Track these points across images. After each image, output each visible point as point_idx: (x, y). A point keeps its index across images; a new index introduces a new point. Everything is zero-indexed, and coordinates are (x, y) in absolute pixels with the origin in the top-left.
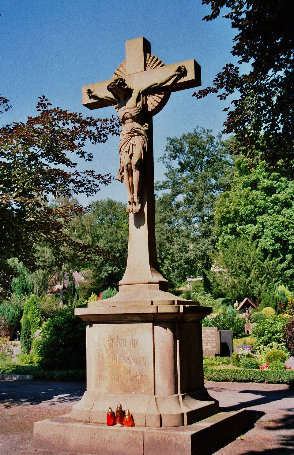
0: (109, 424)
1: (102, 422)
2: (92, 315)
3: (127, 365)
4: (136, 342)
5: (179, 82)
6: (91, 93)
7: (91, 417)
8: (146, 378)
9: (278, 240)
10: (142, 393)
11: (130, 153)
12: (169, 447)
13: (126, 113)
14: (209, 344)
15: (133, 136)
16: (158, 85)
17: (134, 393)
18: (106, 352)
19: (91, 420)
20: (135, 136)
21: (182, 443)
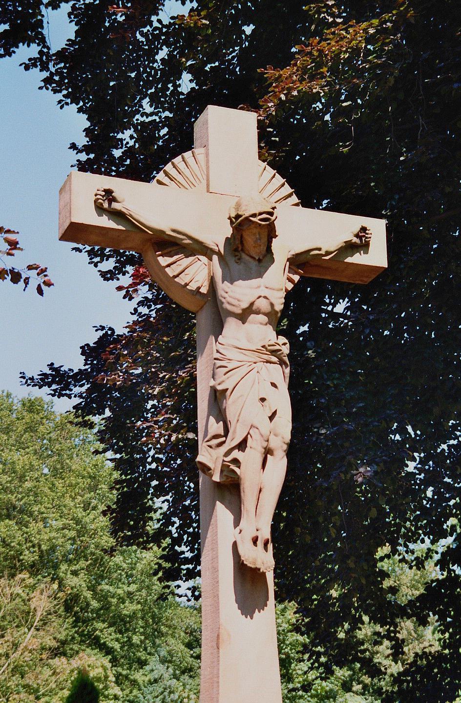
5: (349, 260)
20: (271, 362)
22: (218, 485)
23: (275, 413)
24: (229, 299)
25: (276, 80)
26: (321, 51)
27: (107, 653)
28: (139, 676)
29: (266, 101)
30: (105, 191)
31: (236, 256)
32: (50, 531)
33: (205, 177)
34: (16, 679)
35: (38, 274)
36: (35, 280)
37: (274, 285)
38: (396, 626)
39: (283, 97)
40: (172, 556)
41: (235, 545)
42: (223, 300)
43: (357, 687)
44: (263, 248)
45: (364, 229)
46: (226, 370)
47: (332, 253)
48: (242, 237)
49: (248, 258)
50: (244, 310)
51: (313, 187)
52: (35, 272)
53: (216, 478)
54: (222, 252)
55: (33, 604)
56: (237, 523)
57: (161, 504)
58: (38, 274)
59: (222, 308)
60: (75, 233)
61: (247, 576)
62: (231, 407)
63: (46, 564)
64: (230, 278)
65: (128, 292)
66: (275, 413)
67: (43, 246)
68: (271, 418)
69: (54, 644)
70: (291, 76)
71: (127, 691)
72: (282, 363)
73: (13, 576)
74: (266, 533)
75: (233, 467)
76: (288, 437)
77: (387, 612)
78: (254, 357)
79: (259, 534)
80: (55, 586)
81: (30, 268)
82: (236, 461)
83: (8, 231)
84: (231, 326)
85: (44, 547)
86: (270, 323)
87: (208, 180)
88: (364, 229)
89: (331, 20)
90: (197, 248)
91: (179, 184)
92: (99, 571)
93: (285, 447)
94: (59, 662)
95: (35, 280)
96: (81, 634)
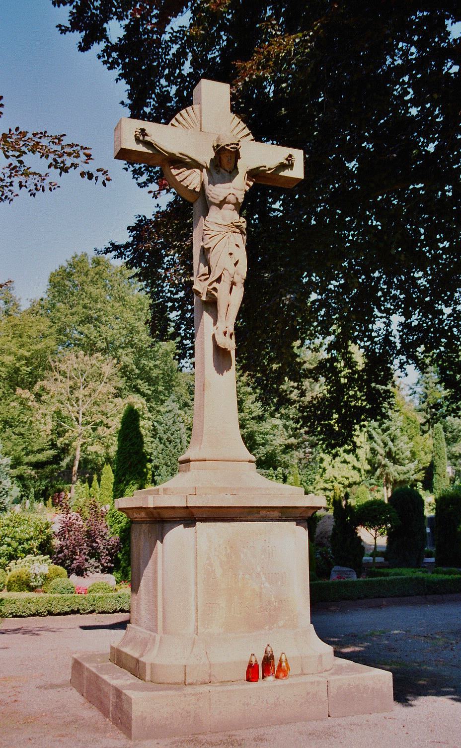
0: (248, 680)
1: (226, 680)
2: (218, 507)
5: (282, 174)
17: (267, 628)
18: (221, 567)
19: (213, 679)
20: (236, 232)
21: (381, 687)
22: (205, 303)
23: (237, 262)
24: (212, 195)
25: (243, 69)
26: (269, 52)
27: (144, 396)
28: (162, 409)
29: (238, 82)
30: (141, 129)
31: (216, 169)
32: (113, 331)
33: (199, 122)
34: (95, 408)
35: (103, 174)
36: (102, 178)
37: (238, 187)
38: (302, 382)
39: (247, 79)
40: (181, 346)
41: (214, 336)
42: (209, 196)
43: (278, 415)
44: (233, 165)
45: (290, 156)
46: (210, 236)
47: (272, 169)
48: (220, 158)
49: (223, 171)
50: (221, 202)
51: (262, 131)
52: (101, 173)
53: (204, 298)
54: (209, 167)
55: (103, 370)
56: (215, 324)
57: (174, 315)
58: (103, 174)
59: (208, 200)
60: (123, 154)
61: (220, 353)
62: (212, 257)
63: (110, 349)
64: (213, 182)
65: (154, 194)
66: (237, 262)
67: (104, 158)
68: (236, 264)
69: (115, 391)
70: (252, 66)
71: (154, 416)
72: (242, 233)
73: (91, 355)
74: (231, 329)
75: (213, 292)
76: (245, 275)
77: (297, 376)
78: (225, 229)
79: (227, 330)
80: (115, 361)
81: (98, 170)
82: (215, 289)
83: (86, 148)
84: (213, 210)
85: (109, 339)
86: (235, 209)
87: (201, 124)
88: (290, 156)
89: (274, 33)
90: (193, 164)
91: (184, 126)
92: (140, 353)
93: (243, 281)
94: (118, 400)
95: (102, 178)
96: (130, 386)
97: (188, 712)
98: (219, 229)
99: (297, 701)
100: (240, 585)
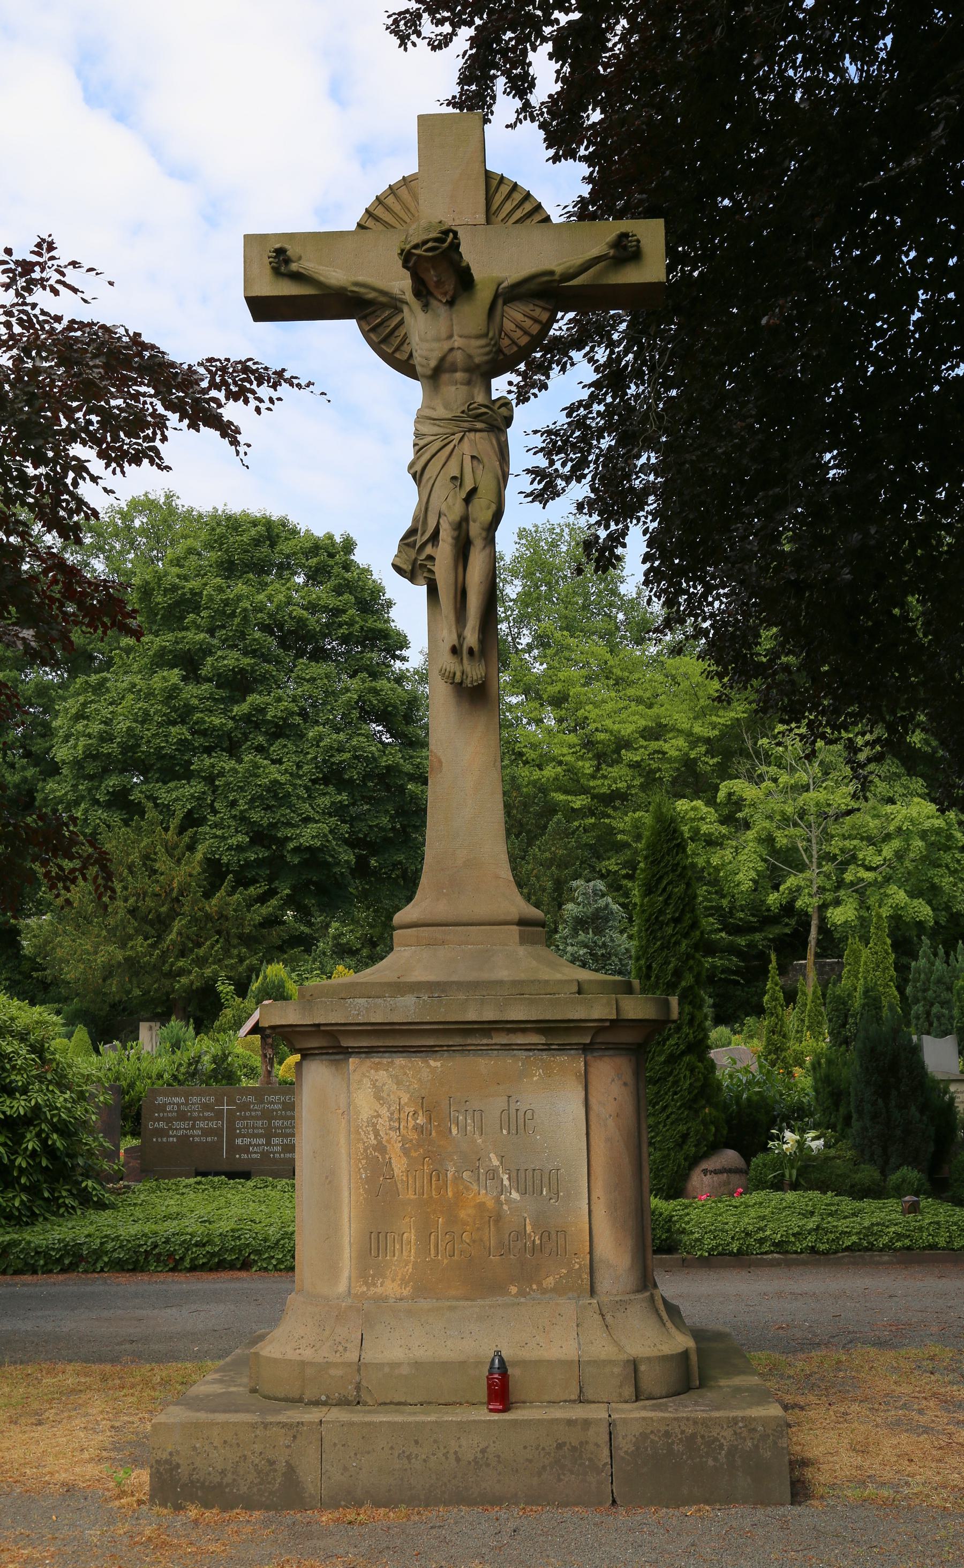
3: (486, 1197)
4: (521, 1121)
6: (287, 261)
7: (364, 1383)
8: (561, 1242)
9: (260, 837)
10: (544, 1291)
11: (468, 486)
12: (711, 1462)
13: (452, 350)
14: (275, 1140)
15: (470, 430)
16: (556, 277)
19: (365, 1396)
20: (476, 431)
21: (756, 1447)
91: (386, 225)
97: (271, 1463)
98: (436, 430)
99: (530, 1461)
100: (450, 1194)
